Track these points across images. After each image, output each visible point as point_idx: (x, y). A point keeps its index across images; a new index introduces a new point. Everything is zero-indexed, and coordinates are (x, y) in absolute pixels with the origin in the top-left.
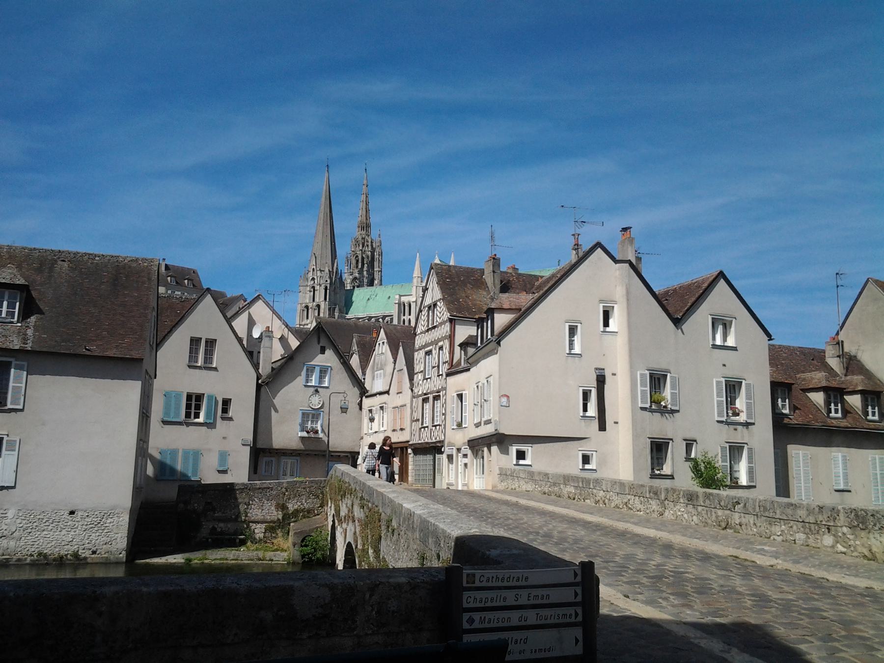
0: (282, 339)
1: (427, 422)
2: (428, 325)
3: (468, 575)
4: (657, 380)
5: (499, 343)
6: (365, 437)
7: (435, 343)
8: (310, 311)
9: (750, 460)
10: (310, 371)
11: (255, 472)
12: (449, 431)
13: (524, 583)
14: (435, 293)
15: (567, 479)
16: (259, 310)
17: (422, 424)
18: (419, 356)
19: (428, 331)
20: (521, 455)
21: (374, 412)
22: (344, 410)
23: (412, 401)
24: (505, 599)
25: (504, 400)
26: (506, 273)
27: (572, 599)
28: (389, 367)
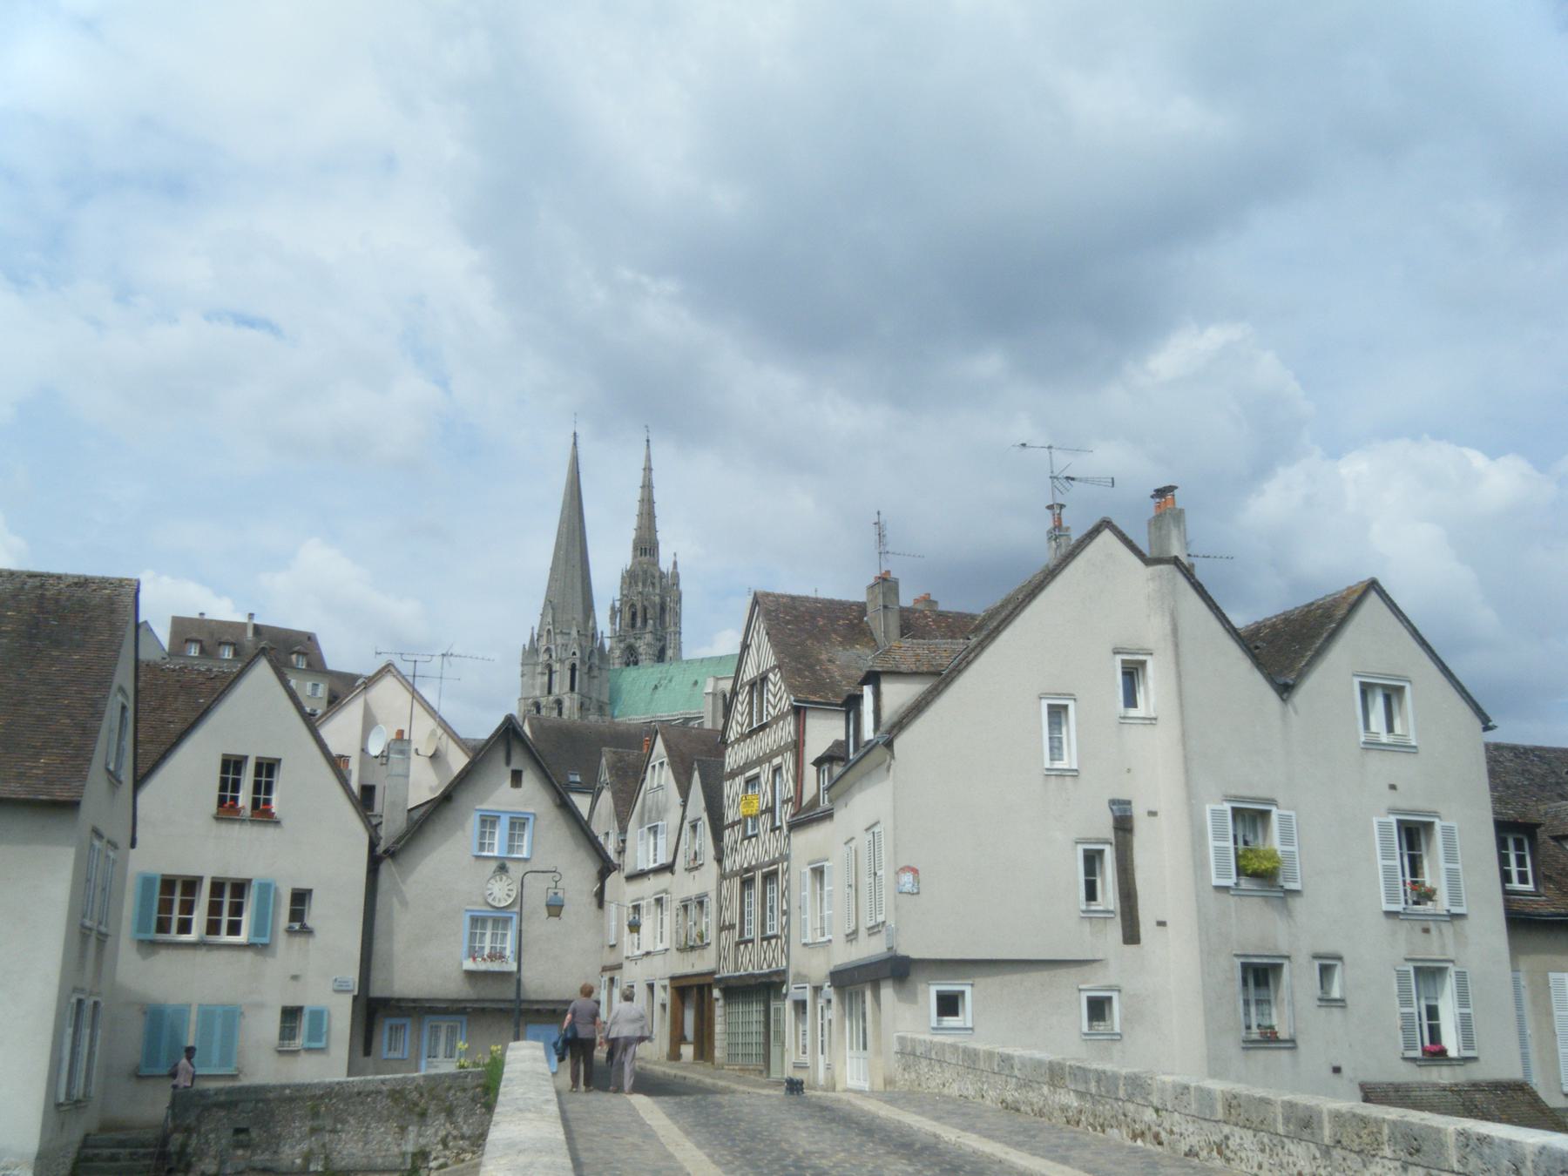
0: (435, 757)
1: (753, 931)
2: (751, 724)
4: (1250, 818)
5: (889, 745)
6: (626, 964)
9: (1463, 998)
10: (489, 821)
11: (367, 1051)
12: (796, 949)
14: (763, 656)
15: (1056, 1074)
16: (388, 695)
17: (742, 933)
20: (949, 1005)
21: (644, 911)
22: (555, 909)
23: (720, 886)
25: (907, 879)
26: (908, 610)
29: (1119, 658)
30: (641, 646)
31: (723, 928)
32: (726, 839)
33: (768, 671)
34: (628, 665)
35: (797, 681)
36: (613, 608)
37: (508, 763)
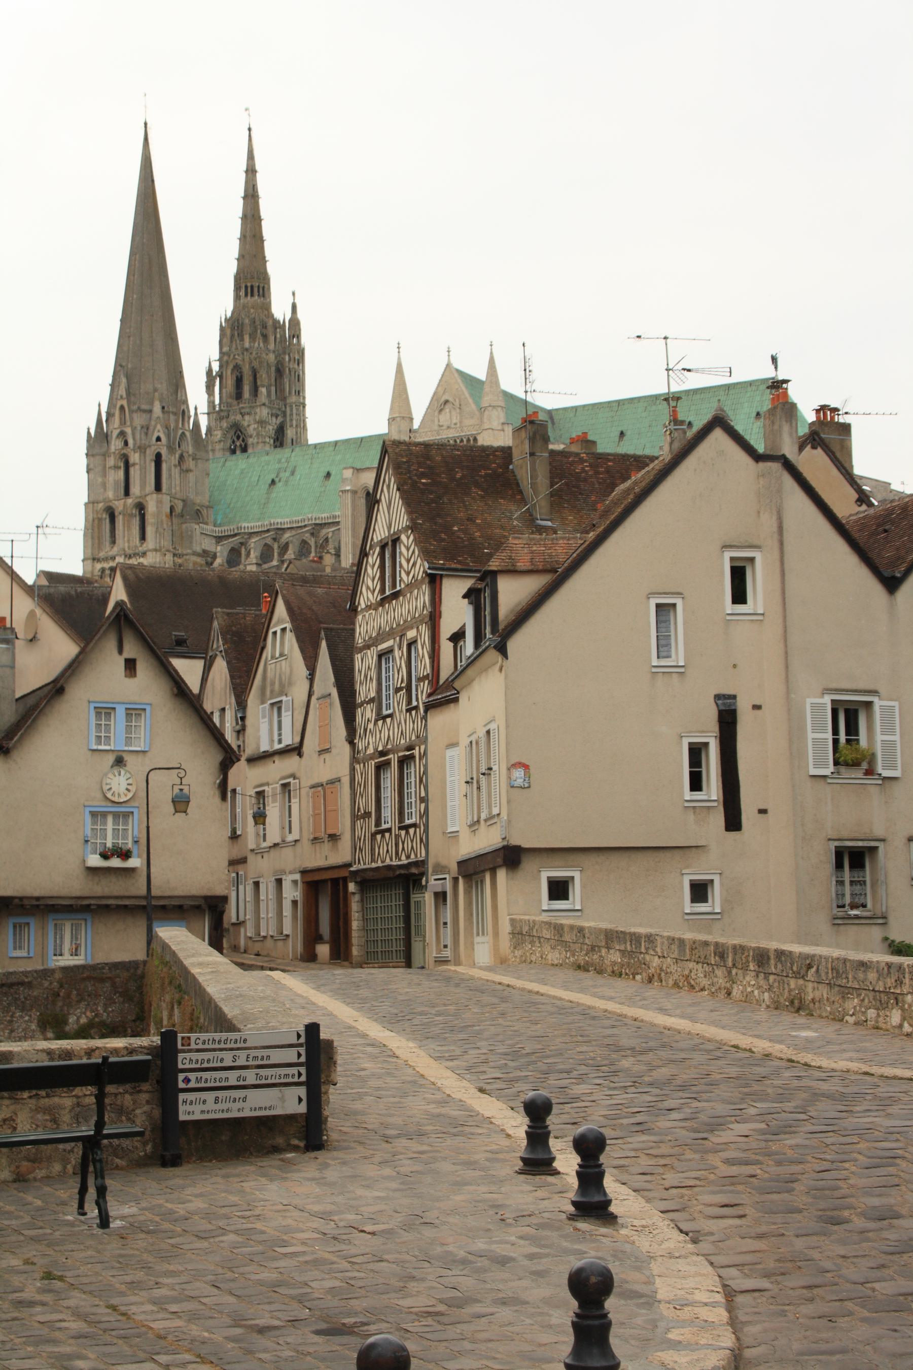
3: (183, 1038)
4: (849, 716)
6: (251, 858)
7: (399, 632)
8: (120, 521)
10: (104, 712)
13: (242, 1045)
14: (392, 515)
17: (378, 824)
18: (365, 662)
19: (382, 602)
20: (559, 890)
21: (269, 800)
23: (353, 770)
24: (222, 1060)
25: (518, 774)
27: (294, 1059)
28: (300, 691)
29: (728, 555)
30: (249, 424)
31: (355, 817)
32: (359, 718)
33: (400, 531)
34: (233, 452)
35: (433, 545)
36: (209, 372)
37: (120, 651)
